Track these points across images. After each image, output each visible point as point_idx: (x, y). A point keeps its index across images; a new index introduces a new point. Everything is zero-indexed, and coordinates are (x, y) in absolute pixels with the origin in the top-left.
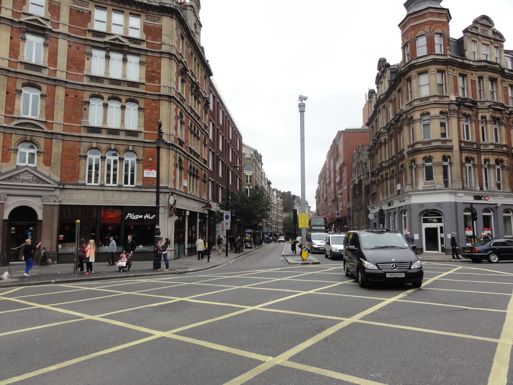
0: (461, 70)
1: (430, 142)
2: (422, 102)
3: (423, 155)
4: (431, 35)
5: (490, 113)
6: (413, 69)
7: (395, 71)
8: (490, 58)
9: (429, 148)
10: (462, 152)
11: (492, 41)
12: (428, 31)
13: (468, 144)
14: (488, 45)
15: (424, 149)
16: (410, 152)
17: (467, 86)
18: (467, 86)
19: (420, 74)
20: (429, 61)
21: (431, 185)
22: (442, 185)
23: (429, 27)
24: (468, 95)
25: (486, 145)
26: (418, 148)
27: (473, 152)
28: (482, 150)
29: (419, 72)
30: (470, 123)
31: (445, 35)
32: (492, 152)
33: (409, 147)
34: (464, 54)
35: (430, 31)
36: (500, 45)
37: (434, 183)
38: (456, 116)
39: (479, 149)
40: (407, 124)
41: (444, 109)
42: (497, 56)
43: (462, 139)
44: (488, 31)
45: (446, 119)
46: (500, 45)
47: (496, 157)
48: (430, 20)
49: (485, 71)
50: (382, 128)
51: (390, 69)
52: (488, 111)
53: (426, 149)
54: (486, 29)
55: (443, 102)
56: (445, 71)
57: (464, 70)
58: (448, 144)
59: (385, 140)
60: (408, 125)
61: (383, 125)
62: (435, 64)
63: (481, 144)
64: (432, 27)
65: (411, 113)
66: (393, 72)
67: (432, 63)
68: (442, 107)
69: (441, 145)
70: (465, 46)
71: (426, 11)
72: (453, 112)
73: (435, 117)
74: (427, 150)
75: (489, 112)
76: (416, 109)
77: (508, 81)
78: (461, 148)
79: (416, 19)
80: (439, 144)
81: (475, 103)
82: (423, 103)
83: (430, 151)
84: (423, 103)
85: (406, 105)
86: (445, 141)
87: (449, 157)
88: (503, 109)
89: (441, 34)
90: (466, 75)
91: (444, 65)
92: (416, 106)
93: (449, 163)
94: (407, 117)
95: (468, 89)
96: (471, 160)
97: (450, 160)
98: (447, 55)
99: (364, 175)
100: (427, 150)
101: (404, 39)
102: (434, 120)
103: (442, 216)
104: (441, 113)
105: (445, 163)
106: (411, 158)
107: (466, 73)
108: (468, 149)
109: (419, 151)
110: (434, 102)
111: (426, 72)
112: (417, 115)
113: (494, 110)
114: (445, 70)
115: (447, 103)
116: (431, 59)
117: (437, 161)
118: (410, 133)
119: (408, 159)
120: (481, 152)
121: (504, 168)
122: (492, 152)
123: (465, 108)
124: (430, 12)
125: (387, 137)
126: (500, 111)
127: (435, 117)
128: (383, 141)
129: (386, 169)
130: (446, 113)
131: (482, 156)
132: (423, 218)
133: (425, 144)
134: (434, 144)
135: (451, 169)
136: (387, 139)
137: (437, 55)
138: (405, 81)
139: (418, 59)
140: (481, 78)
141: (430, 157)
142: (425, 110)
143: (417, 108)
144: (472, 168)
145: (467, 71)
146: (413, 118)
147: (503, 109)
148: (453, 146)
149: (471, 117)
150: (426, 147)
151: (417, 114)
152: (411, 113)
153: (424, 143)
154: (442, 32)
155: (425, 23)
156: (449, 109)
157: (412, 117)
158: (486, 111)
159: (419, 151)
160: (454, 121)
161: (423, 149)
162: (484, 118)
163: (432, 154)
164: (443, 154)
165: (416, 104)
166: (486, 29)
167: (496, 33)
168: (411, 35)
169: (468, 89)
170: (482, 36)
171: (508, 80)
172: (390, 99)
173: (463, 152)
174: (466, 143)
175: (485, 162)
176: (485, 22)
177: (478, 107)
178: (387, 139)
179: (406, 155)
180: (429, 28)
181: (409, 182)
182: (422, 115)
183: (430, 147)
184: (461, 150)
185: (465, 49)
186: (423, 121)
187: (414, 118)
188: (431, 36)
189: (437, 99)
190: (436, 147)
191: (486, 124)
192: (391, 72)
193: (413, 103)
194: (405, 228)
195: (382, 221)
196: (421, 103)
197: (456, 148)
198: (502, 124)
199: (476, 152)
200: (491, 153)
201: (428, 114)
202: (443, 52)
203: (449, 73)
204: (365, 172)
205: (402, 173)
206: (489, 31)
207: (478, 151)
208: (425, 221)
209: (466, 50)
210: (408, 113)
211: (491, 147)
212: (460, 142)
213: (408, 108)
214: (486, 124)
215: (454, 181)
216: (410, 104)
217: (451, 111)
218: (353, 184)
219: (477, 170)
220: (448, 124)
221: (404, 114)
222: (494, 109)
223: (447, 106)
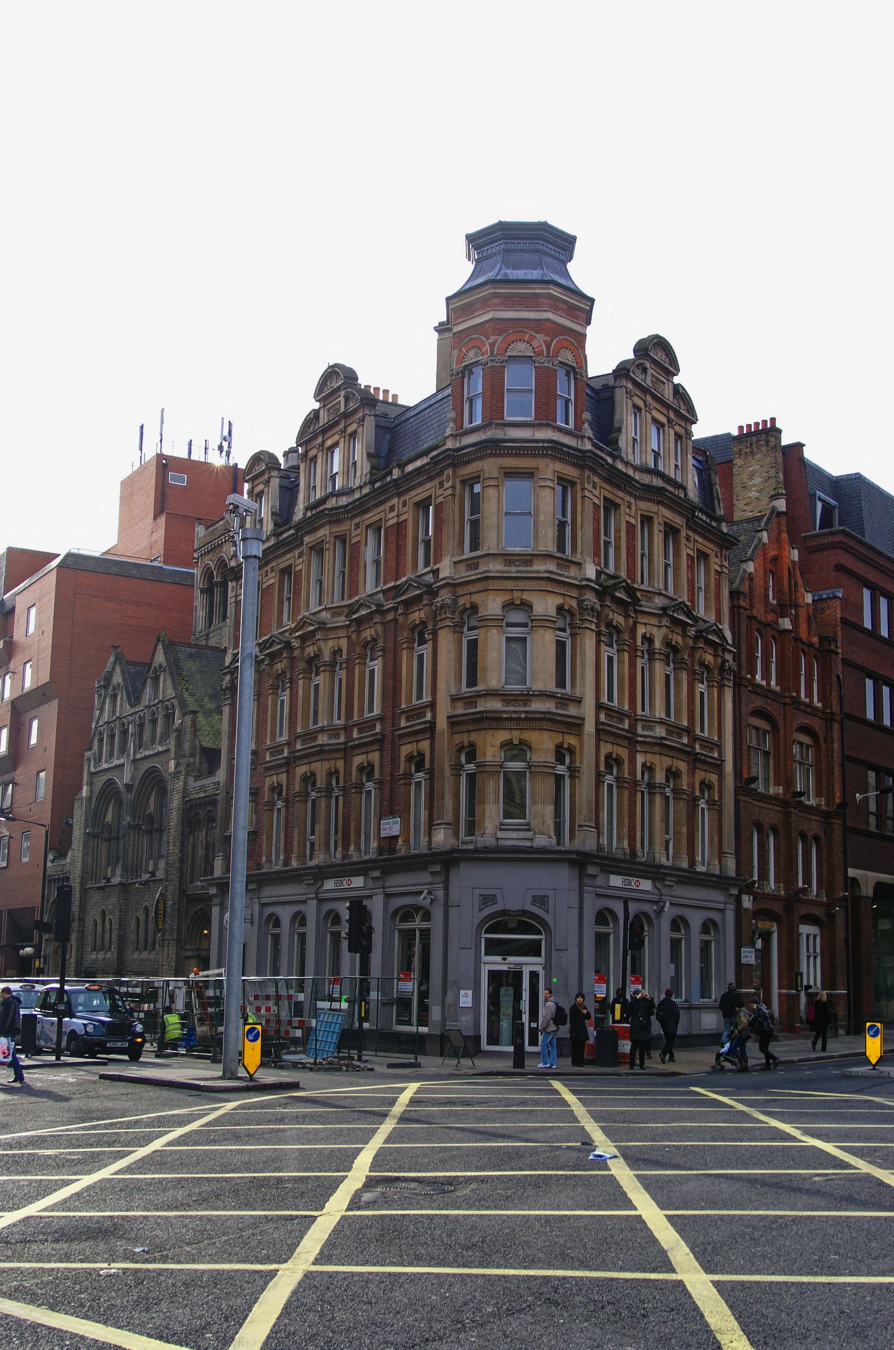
0: (608, 487)
1: (526, 697)
2: (510, 565)
3: (503, 736)
4: (550, 365)
5: (664, 630)
6: (492, 455)
7: (388, 425)
8: (664, 465)
9: (523, 716)
10: (695, 768)
11: (672, 415)
12: (543, 351)
13: (613, 717)
14: (663, 425)
15: (509, 715)
16: (459, 719)
17: (618, 539)
18: (618, 539)
19: (510, 474)
20: (541, 445)
21: (522, 834)
22: (550, 837)
23: (546, 338)
24: (617, 567)
25: (649, 723)
26: (490, 712)
27: (620, 742)
28: (640, 739)
29: (509, 470)
30: (571, 635)
31: (577, 369)
32: (659, 746)
33: (454, 699)
34: (616, 442)
35: (548, 353)
36: (686, 430)
37: (528, 828)
38: (593, 627)
39: (632, 733)
40: (455, 626)
41: (567, 599)
42: (636, 435)
43: (604, 699)
44: (664, 383)
45: (568, 631)
46: (686, 430)
47: (667, 761)
48: (547, 320)
49: (659, 503)
50: (326, 609)
51: (376, 415)
52: (660, 622)
53: (514, 716)
54: (661, 378)
55: (567, 580)
56: (575, 483)
57: (616, 492)
58: (572, 711)
59: (337, 652)
60: (458, 629)
61: (333, 602)
62: (554, 458)
63: (637, 720)
64: (552, 340)
65: (471, 594)
66: (381, 427)
67: (549, 452)
68: (564, 595)
69: (554, 710)
70: (617, 417)
71: (543, 288)
72: (589, 614)
73: (544, 622)
74: (517, 721)
75: (660, 627)
76: (493, 585)
77: (695, 541)
78: (601, 727)
79: (510, 301)
80: (549, 706)
81: (630, 591)
82: (514, 569)
83: (524, 725)
84: (513, 570)
85: (456, 563)
86: (564, 701)
87: (571, 750)
88: (689, 621)
89: (573, 368)
90: (617, 506)
91: (574, 465)
92: (494, 574)
93: (568, 768)
94: (455, 602)
95: (618, 548)
96: (613, 763)
97: (571, 762)
98: (583, 437)
99: (179, 756)
100: (517, 721)
101: (464, 350)
102: (541, 631)
103: (540, 933)
104: (560, 609)
105: (561, 769)
106: (457, 739)
107: (618, 501)
108: (614, 730)
109: (492, 721)
110: (547, 575)
111: (529, 474)
112: (492, 605)
113: (672, 622)
114: (576, 480)
115: (577, 583)
116: (543, 441)
117: (542, 759)
118: (461, 655)
119: (450, 739)
120: (637, 742)
121: (680, 796)
122: (659, 746)
123: (613, 606)
124: (550, 296)
125: (344, 643)
126: (684, 625)
127: (544, 622)
128: (327, 657)
129: (334, 755)
130: (570, 612)
131: (638, 755)
132: (486, 939)
133: (510, 701)
134: (537, 706)
135: (573, 787)
136: (345, 651)
137: (560, 430)
138: (458, 485)
139: (506, 429)
140: (647, 520)
141: (522, 742)
142: (519, 594)
143: (495, 582)
144: (615, 790)
145: (621, 494)
146: (481, 609)
147: (689, 621)
148: (584, 719)
149: (621, 635)
150: (515, 712)
151: (494, 600)
152: (471, 594)
153: (506, 697)
154: (574, 365)
155: (538, 326)
156: (580, 602)
157: (474, 608)
158: (654, 621)
159: (492, 721)
160: (589, 642)
161: (505, 716)
162: (648, 640)
163: (533, 737)
164: (558, 739)
165: (495, 567)
166: (661, 378)
167: (680, 393)
168: (492, 345)
169: (618, 548)
170: (654, 397)
171: (697, 538)
172: (372, 517)
173: (697, 765)
174: (609, 711)
175: (702, 791)
176: (659, 356)
177: (640, 609)
178: (345, 651)
179: (442, 724)
180: (545, 342)
181: (448, 817)
182: (509, 606)
183: (526, 712)
184: (601, 732)
185: (616, 425)
186: (509, 625)
187: (482, 612)
188: (548, 367)
189: (552, 566)
190: (542, 716)
191: (651, 660)
192: (377, 426)
193: (481, 561)
194: (534, 976)
195: (364, 943)
196: (506, 568)
197: (589, 727)
198: (683, 666)
199: (626, 743)
200: (657, 749)
201: (526, 606)
202: (571, 426)
203: (587, 494)
204: (187, 746)
205: (408, 781)
206: (666, 385)
207: (631, 741)
208: (493, 948)
209: (619, 430)
210: (460, 591)
211: (660, 731)
212: (599, 707)
213: (464, 574)
214: (651, 660)
215: (579, 826)
216: (472, 564)
217: (586, 609)
218: (100, 782)
219: (682, 805)
220: (574, 648)
221: (448, 589)
222: (675, 621)
223: (574, 593)
